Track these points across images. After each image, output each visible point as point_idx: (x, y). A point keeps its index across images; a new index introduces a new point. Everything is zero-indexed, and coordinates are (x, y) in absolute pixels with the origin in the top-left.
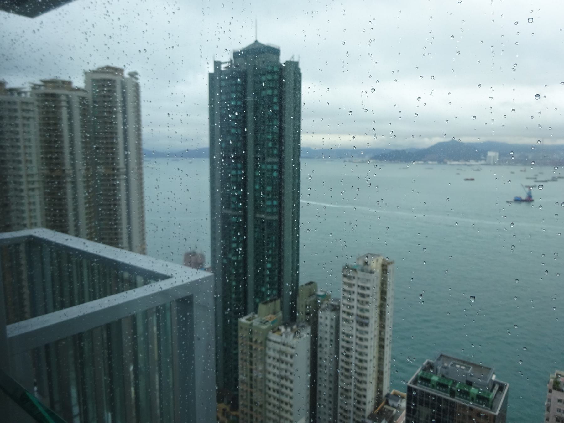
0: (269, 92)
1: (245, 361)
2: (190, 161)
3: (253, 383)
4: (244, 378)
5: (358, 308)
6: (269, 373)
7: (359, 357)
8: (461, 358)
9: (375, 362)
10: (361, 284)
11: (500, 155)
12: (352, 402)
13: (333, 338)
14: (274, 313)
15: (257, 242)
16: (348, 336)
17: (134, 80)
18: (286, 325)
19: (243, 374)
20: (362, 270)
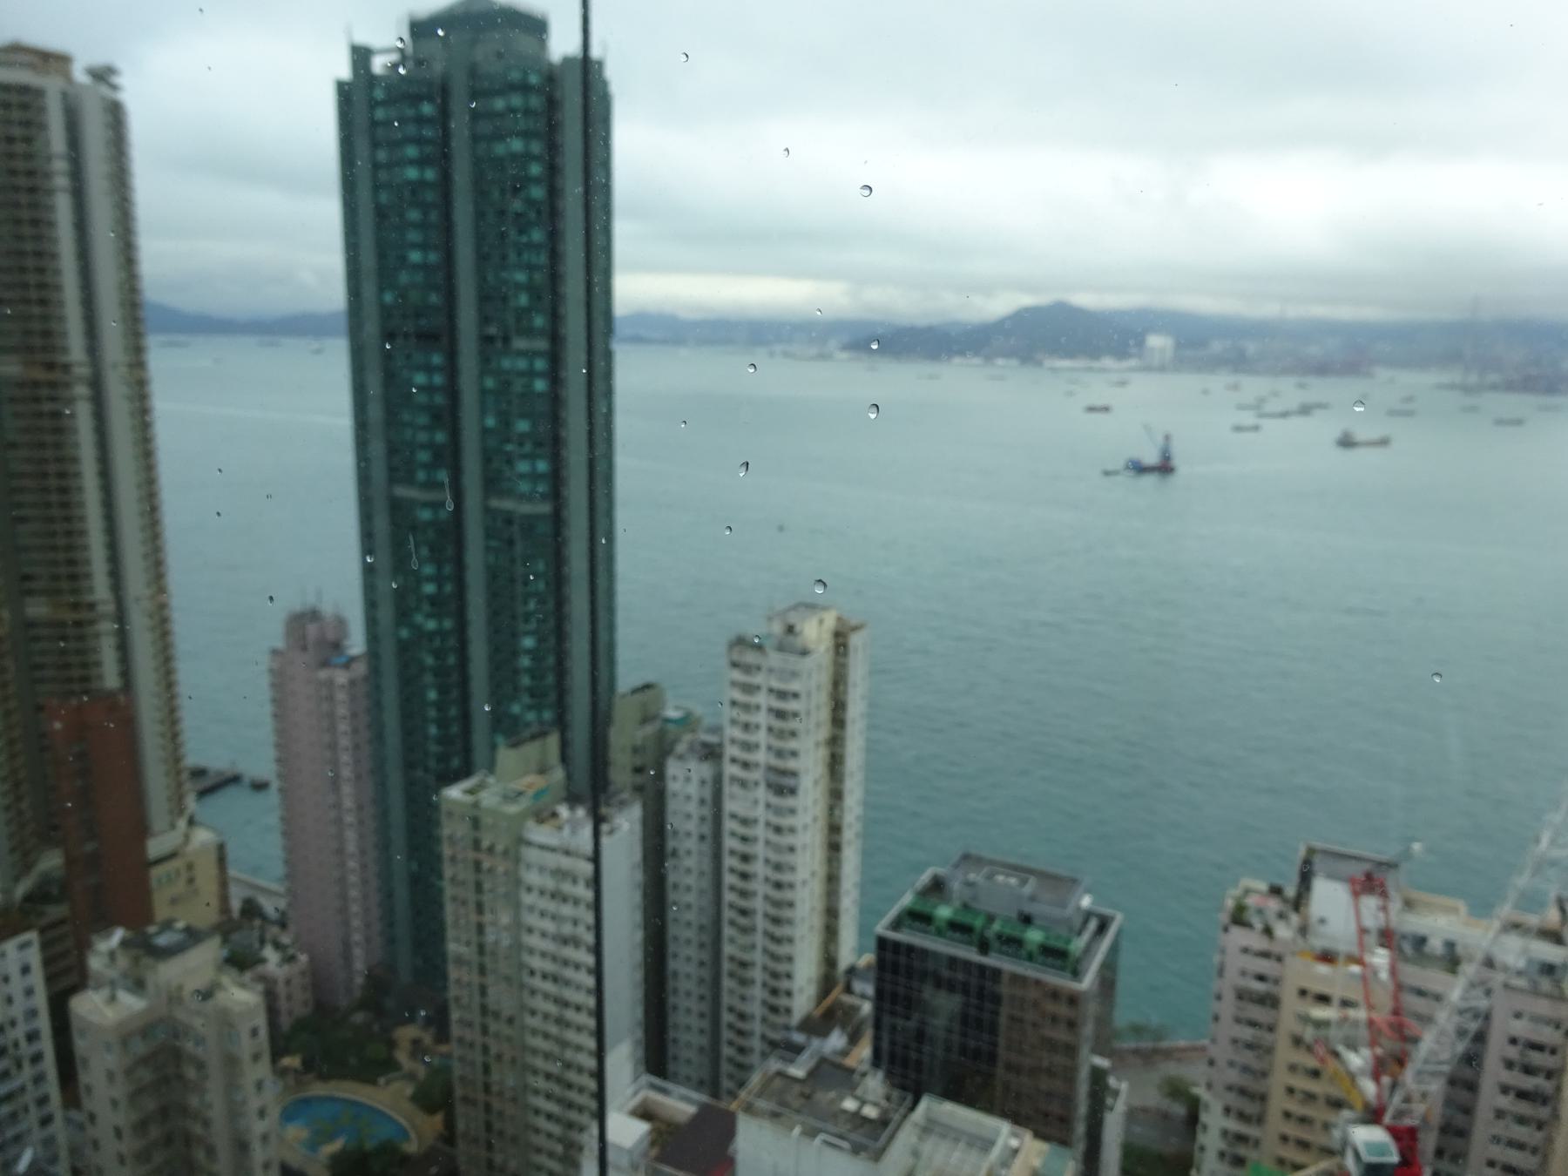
0: (517, 145)
1: (464, 903)
3: (487, 960)
4: (463, 950)
5: (769, 748)
6: (530, 930)
8: (1013, 860)
10: (776, 684)
11: (1179, 346)
14: (543, 770)
16: (745, 822)
17: (104, 90)
18: (572, 799)
19: (457, 940)
20: (781, 648)
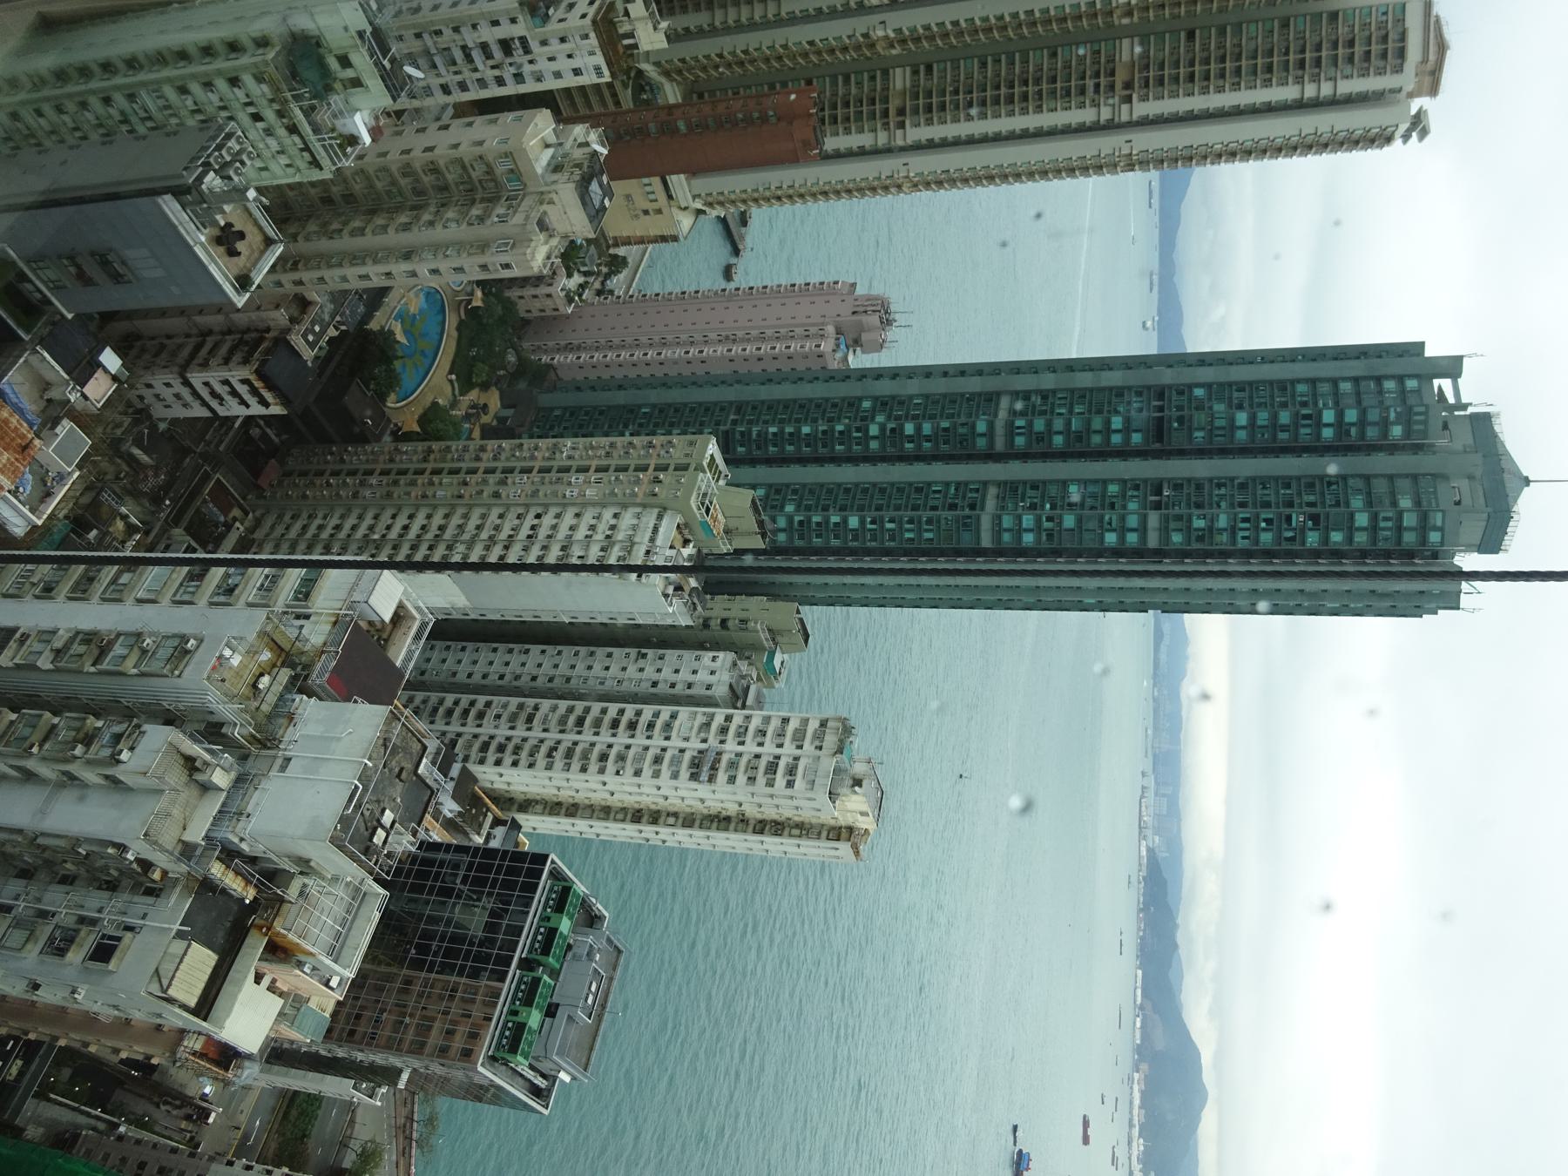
0: (1362, 520)
2: (1149, 324)
3: (554, 475)
5: (739, 755)
7: (613, 753)
9: (600, 797)
12: (503, 732)
13: (662, 688)
15: (919, 490)
16: (668, 726)
20: (837, 771)
